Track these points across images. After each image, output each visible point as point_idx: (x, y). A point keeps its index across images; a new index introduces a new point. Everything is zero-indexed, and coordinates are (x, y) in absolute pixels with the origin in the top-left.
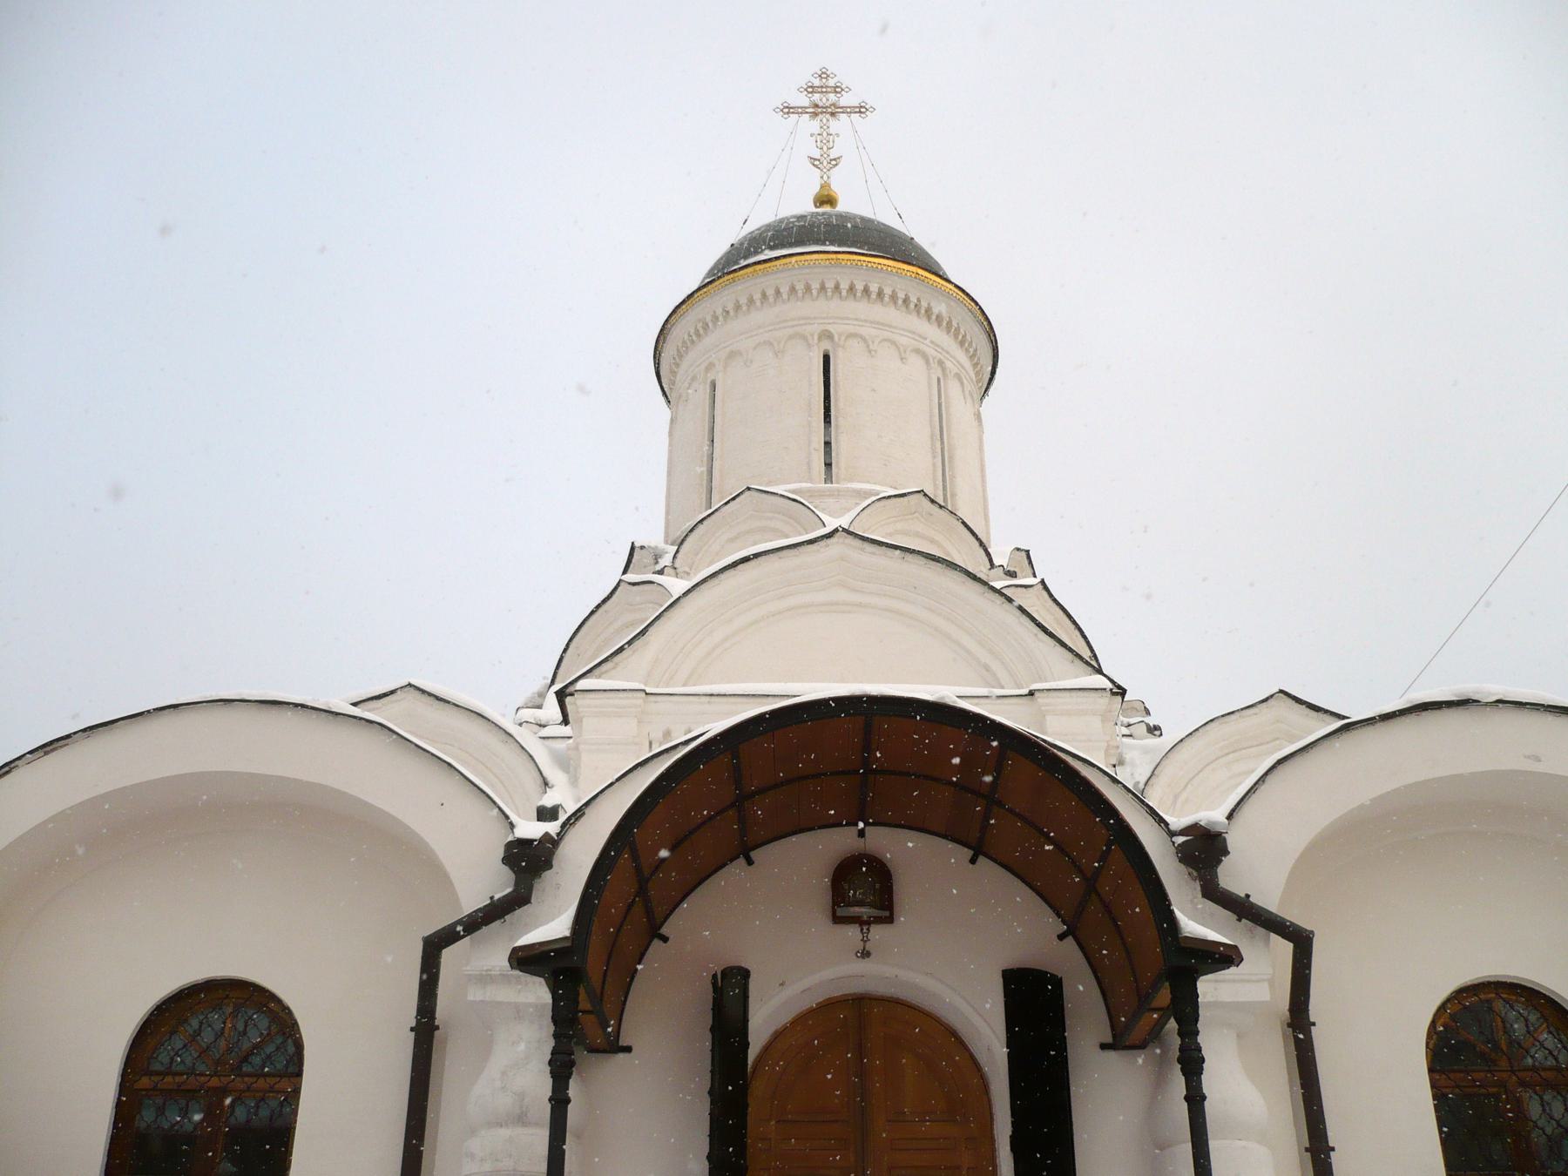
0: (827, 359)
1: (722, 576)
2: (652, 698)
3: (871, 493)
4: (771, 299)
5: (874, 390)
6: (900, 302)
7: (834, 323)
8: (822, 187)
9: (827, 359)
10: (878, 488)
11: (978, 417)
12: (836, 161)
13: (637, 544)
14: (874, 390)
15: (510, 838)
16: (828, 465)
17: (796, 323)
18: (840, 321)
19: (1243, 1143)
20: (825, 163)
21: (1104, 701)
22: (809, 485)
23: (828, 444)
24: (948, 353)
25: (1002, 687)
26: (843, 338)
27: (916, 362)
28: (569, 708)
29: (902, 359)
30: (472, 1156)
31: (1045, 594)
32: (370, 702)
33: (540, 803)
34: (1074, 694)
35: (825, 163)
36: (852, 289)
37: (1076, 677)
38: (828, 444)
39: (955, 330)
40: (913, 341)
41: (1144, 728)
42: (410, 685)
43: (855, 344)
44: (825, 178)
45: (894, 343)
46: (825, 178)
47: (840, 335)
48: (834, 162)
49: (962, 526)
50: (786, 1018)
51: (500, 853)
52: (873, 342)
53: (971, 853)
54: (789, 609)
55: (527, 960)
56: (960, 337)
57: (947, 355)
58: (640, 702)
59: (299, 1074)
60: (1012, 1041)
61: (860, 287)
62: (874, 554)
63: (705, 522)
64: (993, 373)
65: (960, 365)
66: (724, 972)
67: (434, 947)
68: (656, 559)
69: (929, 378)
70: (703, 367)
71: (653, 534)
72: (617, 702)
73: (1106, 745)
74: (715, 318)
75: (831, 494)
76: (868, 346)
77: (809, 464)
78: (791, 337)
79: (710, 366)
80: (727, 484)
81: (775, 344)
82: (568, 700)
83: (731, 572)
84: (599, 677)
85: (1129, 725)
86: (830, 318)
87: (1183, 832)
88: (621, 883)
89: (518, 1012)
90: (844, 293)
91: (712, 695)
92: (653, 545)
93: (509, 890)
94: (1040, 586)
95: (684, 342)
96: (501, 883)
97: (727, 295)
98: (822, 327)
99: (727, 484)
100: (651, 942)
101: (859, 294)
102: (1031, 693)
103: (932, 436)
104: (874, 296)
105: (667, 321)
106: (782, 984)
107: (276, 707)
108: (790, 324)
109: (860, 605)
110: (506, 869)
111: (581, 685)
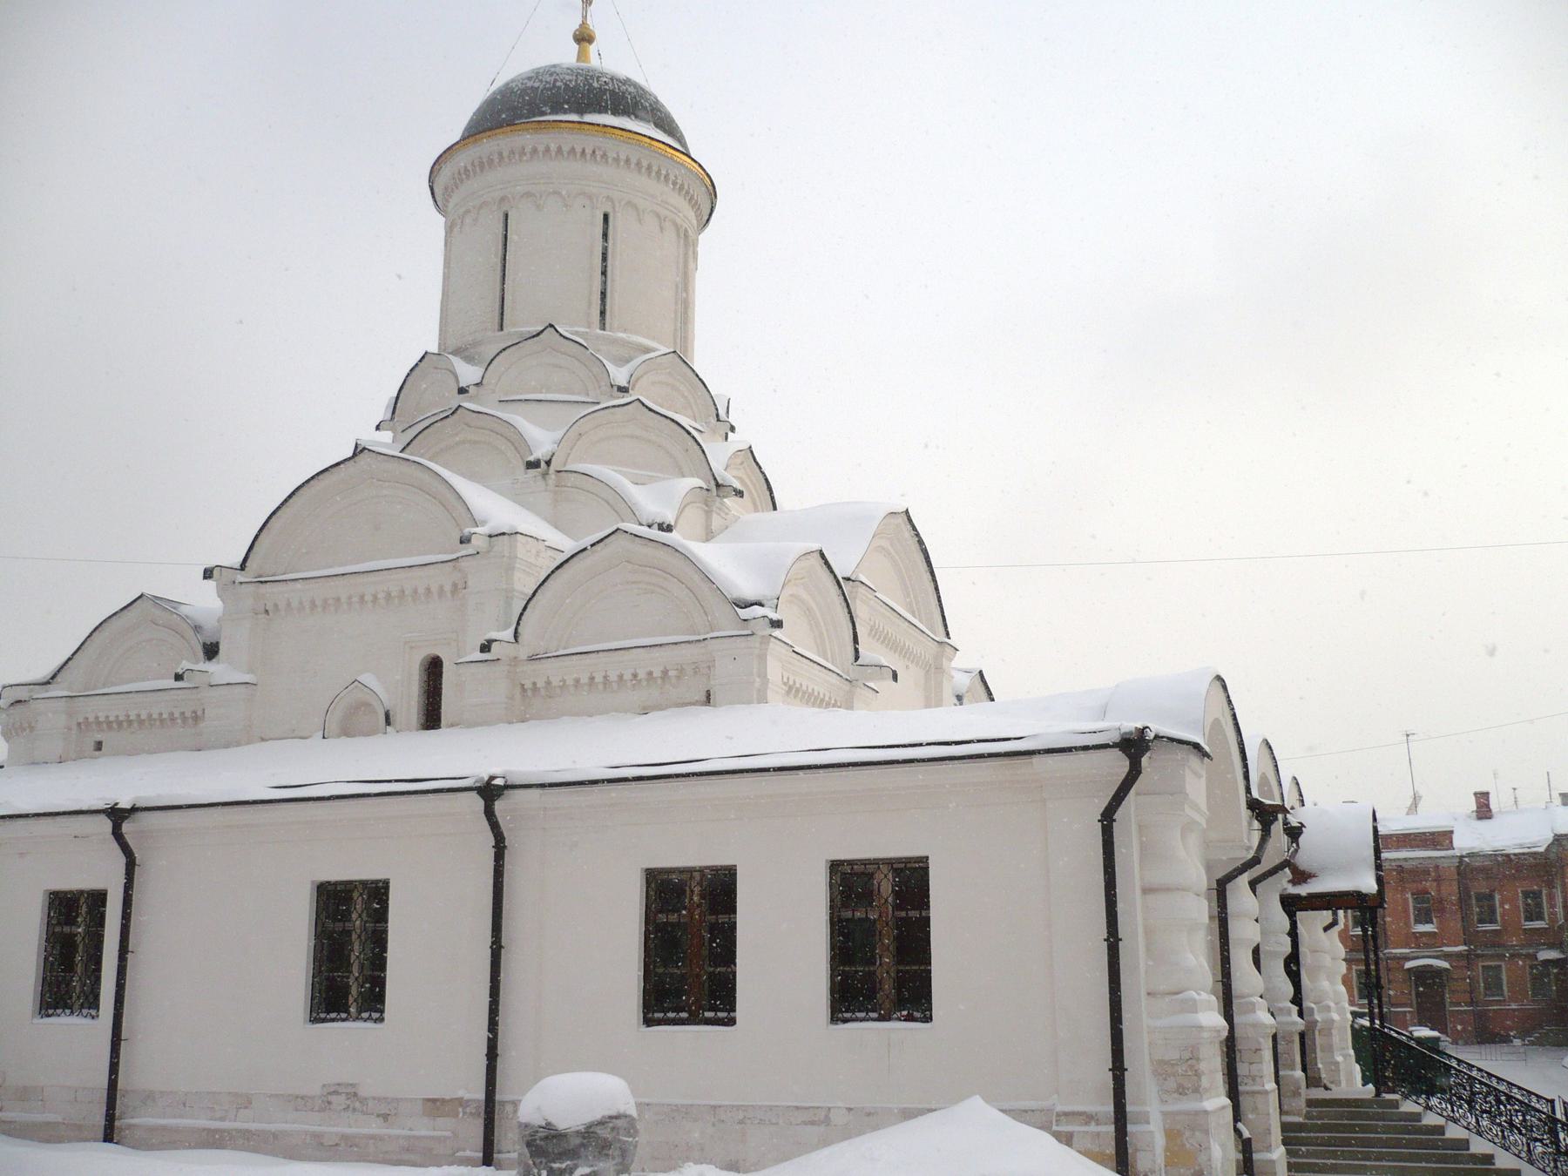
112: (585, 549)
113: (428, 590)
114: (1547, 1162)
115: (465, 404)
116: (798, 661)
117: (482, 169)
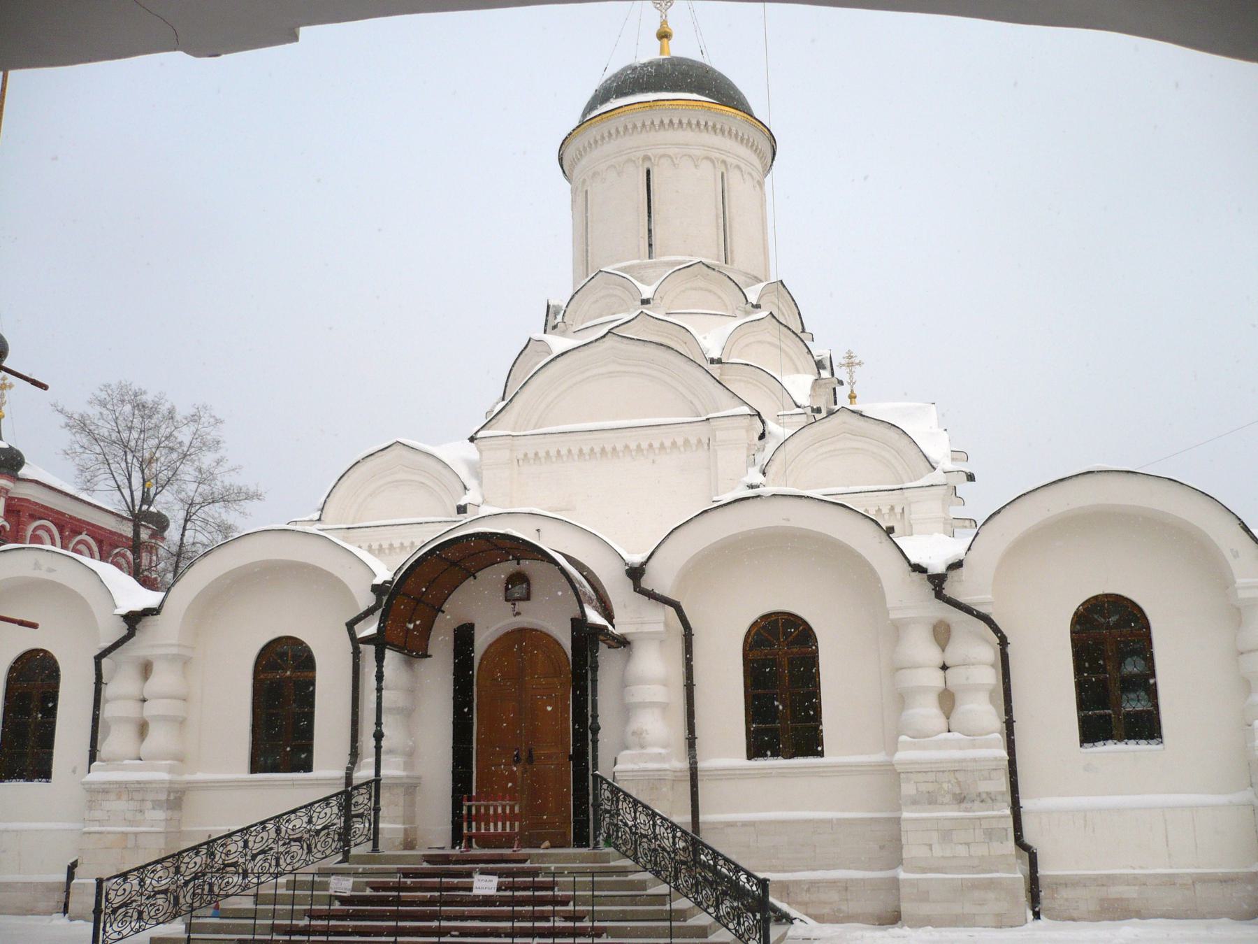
0: (648, 172)
1: (549, 365)
4: (614, 136)
9: (648, 172)
10: (680, 258)
16: (650, 245)
19: (648, 686)
20: (663, 4)
22: (638, 261)
23: (650, 231)
24: (729, 152)
26: (657, 159)
27: (706, 165)
31: (774, 320)
32: (379, 453)
33: (458, 504)
34: (730, 418)
37: (734, 408)
41: (810, 409)
45: (690, 156)
47: (655, 157)
49: (728, 279)
50: (491, 640)
52: (676, 159)
57: (729, 154)
63: (579, 293)
72: (500, 442)
74: (596, 142)
75: (655, 265)
76: (673, 161)
77: (639, 246)
81: (617, 166)
83: (553, 363)
91: (545, 434)
97: (593, 132)
101: (667, 127)
102: (708, 419)
103: (717, 216)
109: (625, 372)
110: (372, 593)
111: (479, 435)
112: (358, 462)
113: (603, 450)
114: (732, 917)
115: (645, 311)
116: (865, 497)
117: (590, 148)
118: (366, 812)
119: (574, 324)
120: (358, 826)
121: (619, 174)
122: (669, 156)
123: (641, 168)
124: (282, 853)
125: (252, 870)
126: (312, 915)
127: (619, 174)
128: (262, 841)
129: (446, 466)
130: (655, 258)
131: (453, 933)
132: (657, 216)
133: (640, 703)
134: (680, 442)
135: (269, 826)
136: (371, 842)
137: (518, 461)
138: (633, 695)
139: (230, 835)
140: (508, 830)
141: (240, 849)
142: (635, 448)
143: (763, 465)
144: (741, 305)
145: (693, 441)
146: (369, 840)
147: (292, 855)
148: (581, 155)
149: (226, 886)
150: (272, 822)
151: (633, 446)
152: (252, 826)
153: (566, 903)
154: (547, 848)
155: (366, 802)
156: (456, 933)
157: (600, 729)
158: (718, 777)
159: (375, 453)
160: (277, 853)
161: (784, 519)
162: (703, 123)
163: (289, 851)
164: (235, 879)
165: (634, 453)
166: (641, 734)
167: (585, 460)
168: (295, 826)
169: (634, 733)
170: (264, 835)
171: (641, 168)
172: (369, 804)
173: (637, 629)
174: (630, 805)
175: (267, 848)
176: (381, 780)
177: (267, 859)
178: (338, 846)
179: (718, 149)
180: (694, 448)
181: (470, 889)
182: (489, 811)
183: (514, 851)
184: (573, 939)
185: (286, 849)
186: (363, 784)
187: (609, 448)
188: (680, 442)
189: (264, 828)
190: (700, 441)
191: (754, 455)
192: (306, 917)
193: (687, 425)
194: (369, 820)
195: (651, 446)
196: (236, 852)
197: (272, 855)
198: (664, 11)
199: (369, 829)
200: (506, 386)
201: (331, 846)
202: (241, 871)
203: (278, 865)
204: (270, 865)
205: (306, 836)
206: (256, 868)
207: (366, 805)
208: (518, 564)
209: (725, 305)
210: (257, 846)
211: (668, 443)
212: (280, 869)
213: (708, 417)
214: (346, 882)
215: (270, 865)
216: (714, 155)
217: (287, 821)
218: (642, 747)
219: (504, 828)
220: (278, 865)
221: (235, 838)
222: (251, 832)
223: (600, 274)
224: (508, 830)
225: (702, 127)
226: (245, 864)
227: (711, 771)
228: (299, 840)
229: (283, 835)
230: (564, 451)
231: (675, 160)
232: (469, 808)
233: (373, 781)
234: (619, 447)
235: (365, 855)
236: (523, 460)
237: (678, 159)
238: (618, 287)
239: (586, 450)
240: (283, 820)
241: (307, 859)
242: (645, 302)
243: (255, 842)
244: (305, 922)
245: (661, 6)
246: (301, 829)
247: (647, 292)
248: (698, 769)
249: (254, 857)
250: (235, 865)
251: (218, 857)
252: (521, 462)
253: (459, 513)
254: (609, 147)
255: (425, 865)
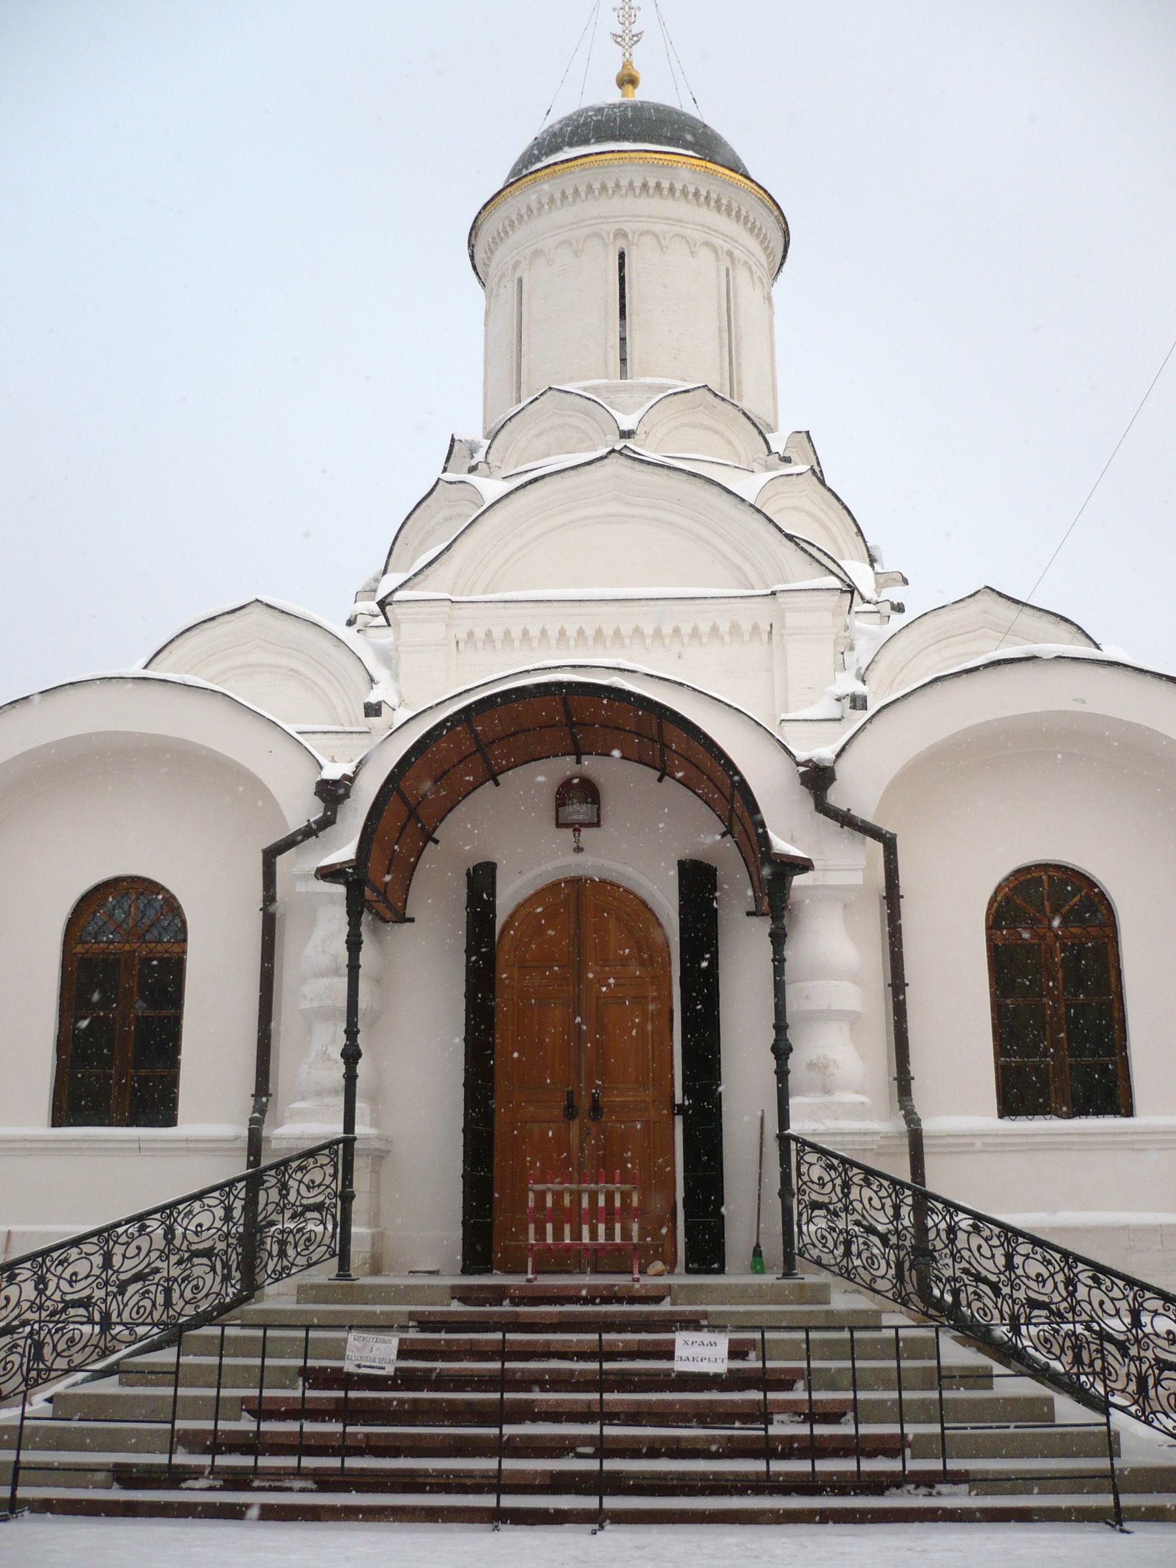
0: (622, 256)
1: (512, 496)
2: (457, 605)
3: (661, 388)
5: (665, 286)
6: (690, 196)
7: (629, 221)
8: (624, 66)
9: (622, 256)
10: (671, 382)
11: (769, 298)
12: (637, 38)
13: (456, 437)
14: (665, 286)
15: (319, 779)
16: (623, 360)
17: (590, 222)
18: (634, 219)
19: (837, 983)
20: (627, 39)
21: (834, 599)
23: (623, 339)
24: (736, 242)
25: (753, 588)
26: (636, 237)
27: (705, 253)
28: (389, 615)
29: (692, 253)
30: (304, 996)
32: (227, 616)
34: (809, 593)
35: (627, 39)
36: (645, 186)
38: (623, 339)
39: (745, 217)
40: (703, 234)
41: (888, 605)
42: (257, 600)
43: (647, 239)
44: (627, 55)
45: (683, 237)
46: (627, 55)
48: (635, 39)
49: (742, 416)
51: (313, 789)
53: (658, 774)
54: (572, 522)
55: (328, 874)
56: (749, 225)
57: (736, 245)
58: (447, 609)
59: (185, 940)
60: (683, 910)
61: (652, 184)
62: (643, 471)
63: (513, 420)
64: (784, 257)
65: (750, 252)
66: (474, 868)
67: (270, 856)
68: (472, 454)
69: (718, 270)
70: (510, 265)
71: (472, 430)
73: (834, 636)
75: (631, 389)
76: (660, 242)
78: (588, 237)
79: (516, 266)
80: (535, 382)
82: (388, 608)
84: (412, 588)
85: (877, 603)
86: (627, 216)
87: (805, 764)
88: (394, 808)
89: (331, 899)
90: (637, 191)
91: (506, 601)
92: (469, 439)
93: (320, 815)
94: (810, 473)
95: (493, 238)
96: (313, 810)
97: (529, 196)
98: (616, 226)
99: (535, 382)
100: (483, 783)
101: (651, 191)
102: (773, 593)
104: (665, 192)
105: (477, 218)
106: (520, 872)
107: (145, 682)
108: (587, 223)
109: (632, 516)
110: (317, 799)
111: (398, 596)
115: (628, 445)
118: (328, 1201)
119: (503, 467)
120: (314, 1228)
121: (577, 254)
122: (655, 235)
123: (611, 247)
124: (176, 1280)
125: (120, 1315)
126: (261, 1410)
127: (577, 254)
128: (138, 1255)
129: (338, 643)
130: (631, 378)
131: (581, 1450)
132: (635, 317)
133: (822, 1011)
134: (724, 627)
135: (153, 1224)
136: (337, 1258)
137: (457, 642)
138: (807, 997)
139: (77, 1242)
140: (618, 1240)
141: (96, 1271)
142: (652, 632)
143: (860, 668)
144: (761, 455)
145: (746, 627)
146: (333, 1255)
147: (195, 1282)
148: (506, 233)
149: (69, 1348)
150: (158, 1216)
151: (648, 629)
152: (119, 1225)
153: (788, 1386)
154: (660, 1274)
155: (328, 1180)
156: (589, 1450)
157: (791, 1049)
158: (953, 1149)
159: (219, 616)
160: (168, 1280)
161: (1076, 700)
162: (703, 193)
163: (189, 1276)
164: (87, 1329)
165: (649, 641)
166: (826, 1067)
167: (568, 647)
168: (200, 1225)
169: (811, 1066)
170: (144, 1242)
171: (611, 247)
172: (333, 1186)
173: (815, 880)
174: (883, 1193)
175: (147, 1270)
176: (355, 1139)
177: (148, 1292)
178: (279, 1268)
179: (722, 234)
180: (746, 638)
181: (669, 1355)
182: (639, 1200)
183: (529, 1280)
184: (948, 1467)
185: (185, 1270)
186: (324, 1147)
187: (608, 631)
188: (724, 627)
189: (143, 1228)
190: (755, 628)
191: (843, 653)
192: (245, 1414)
193: (738, 600)
194: (334, 1217)
195: (676, 631)
196: (87, 1277)
197: (158, 1284)
198: (627, 47)
199: (333, 1236)
200: (390, 554)
201: (266, 1265)
202: (97, 1317)
203: (168, 1303)
204: (154, 1305)
205: (99, 1294)
206: (127, 1309)
207: (328, 1187)
208: (578, 762)
209: (738, 456)
210: (129, 1264)
211: (705, 628)
212: (171, 1313)
213: (774, 589)
214: (383, 1346)
215: (154, 1305)
216: (718, 241)
217: (186, 1216)
218: (827, 1090)
219: (610, 1234)
220: (168, 1303)
221: (87, 1248)
222: (118, 1237)
223: (549, 393)
224: (618, 1240)
225: (702, 199)
226: (105, 1301)
227: (940, 1137)
228: (208, 1253)
229: (177, 1242)
230: (534, 632)
231: (662, 240)
232: (540, 1196)
233: (337, 1142)
234: (626, 629)
235: (326, 1286)
236: (466, 643)
237: (667, 240)
238: (578, 414)
239: (571, 632)
240: (179, 1213)
241: (223, 1292)
242: (626, 434)
243: (124, 1256)
244: (247, 1424)
245: (624, 40)
246: (213, 1231)
247: (627, 423)
248: (923, 1134)
249: (122, 1287)
250: (86, 1303)
251: (52, 1286)
252: (461, 645)
253: (367, 715)
254: (563, 215)
255: (456, 1306)
